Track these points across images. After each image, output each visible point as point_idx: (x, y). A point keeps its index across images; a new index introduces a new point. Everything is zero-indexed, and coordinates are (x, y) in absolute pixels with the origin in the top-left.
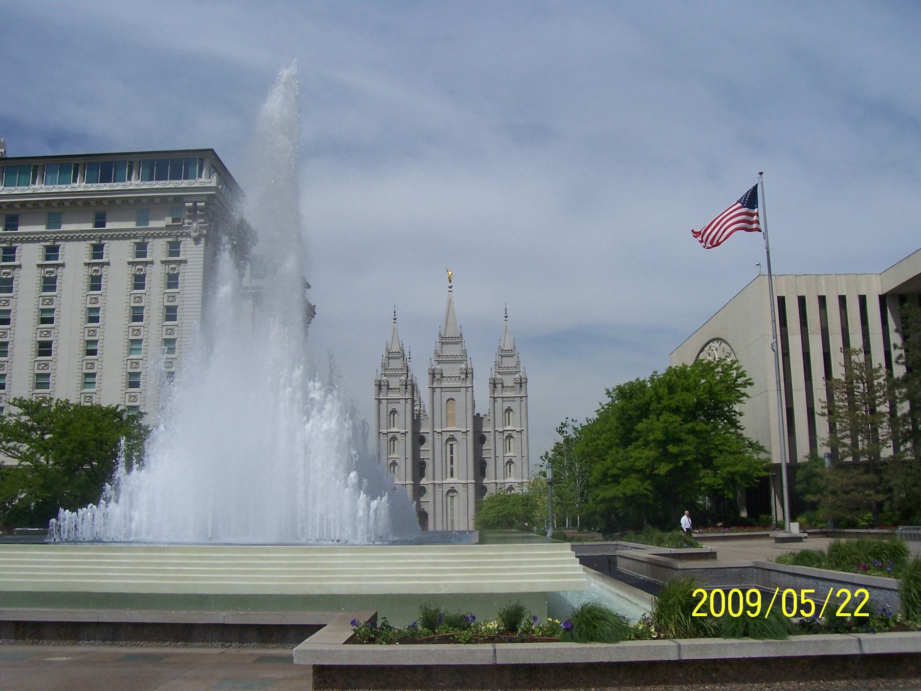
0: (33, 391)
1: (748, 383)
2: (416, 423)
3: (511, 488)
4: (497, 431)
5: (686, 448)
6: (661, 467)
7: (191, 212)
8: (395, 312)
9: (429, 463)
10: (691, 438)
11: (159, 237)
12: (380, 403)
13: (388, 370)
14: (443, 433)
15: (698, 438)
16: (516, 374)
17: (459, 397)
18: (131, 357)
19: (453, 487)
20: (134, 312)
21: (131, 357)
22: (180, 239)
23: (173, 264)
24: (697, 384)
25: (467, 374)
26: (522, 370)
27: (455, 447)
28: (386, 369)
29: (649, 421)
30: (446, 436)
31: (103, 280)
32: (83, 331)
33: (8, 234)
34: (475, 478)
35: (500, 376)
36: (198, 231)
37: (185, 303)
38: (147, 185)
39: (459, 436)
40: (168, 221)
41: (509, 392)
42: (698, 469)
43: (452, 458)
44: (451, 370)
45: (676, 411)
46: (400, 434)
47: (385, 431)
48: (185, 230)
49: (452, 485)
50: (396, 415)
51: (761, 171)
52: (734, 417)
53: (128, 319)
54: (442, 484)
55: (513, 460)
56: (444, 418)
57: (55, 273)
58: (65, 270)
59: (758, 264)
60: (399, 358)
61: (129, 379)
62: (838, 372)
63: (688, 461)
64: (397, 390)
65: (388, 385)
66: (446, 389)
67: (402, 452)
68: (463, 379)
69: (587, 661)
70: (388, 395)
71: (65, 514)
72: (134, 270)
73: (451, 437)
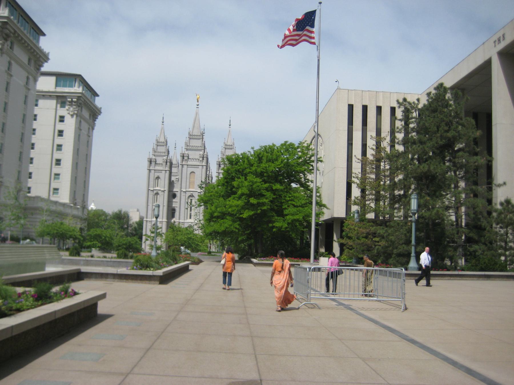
1: (319, 160)
2: (171, 184)
4: (182, 191)
5: (265, 200)
6: (245, 213)
9: (177, 210)
10: (268, 194)
14: (187, 192)
15: (274, 194)
16: (165, 156)
24: (278, 157)
25: (203, 158)
29: (239, 180)
30: (188, 194)
34: (168, 219)
42: (273, 216)
44: (193, 154)
45: (261, 175)
47: (152, 189)
51: (320, 1)
52: (308, 184)
54: (184, 222)
56: (188, 183)
59: (336, 81)
60: (163, 146)
62: (370, 153)
63: (264, 210)
65: (156, 162)
66: (190, 166)
68: (201, 161)
73: (191, 195)
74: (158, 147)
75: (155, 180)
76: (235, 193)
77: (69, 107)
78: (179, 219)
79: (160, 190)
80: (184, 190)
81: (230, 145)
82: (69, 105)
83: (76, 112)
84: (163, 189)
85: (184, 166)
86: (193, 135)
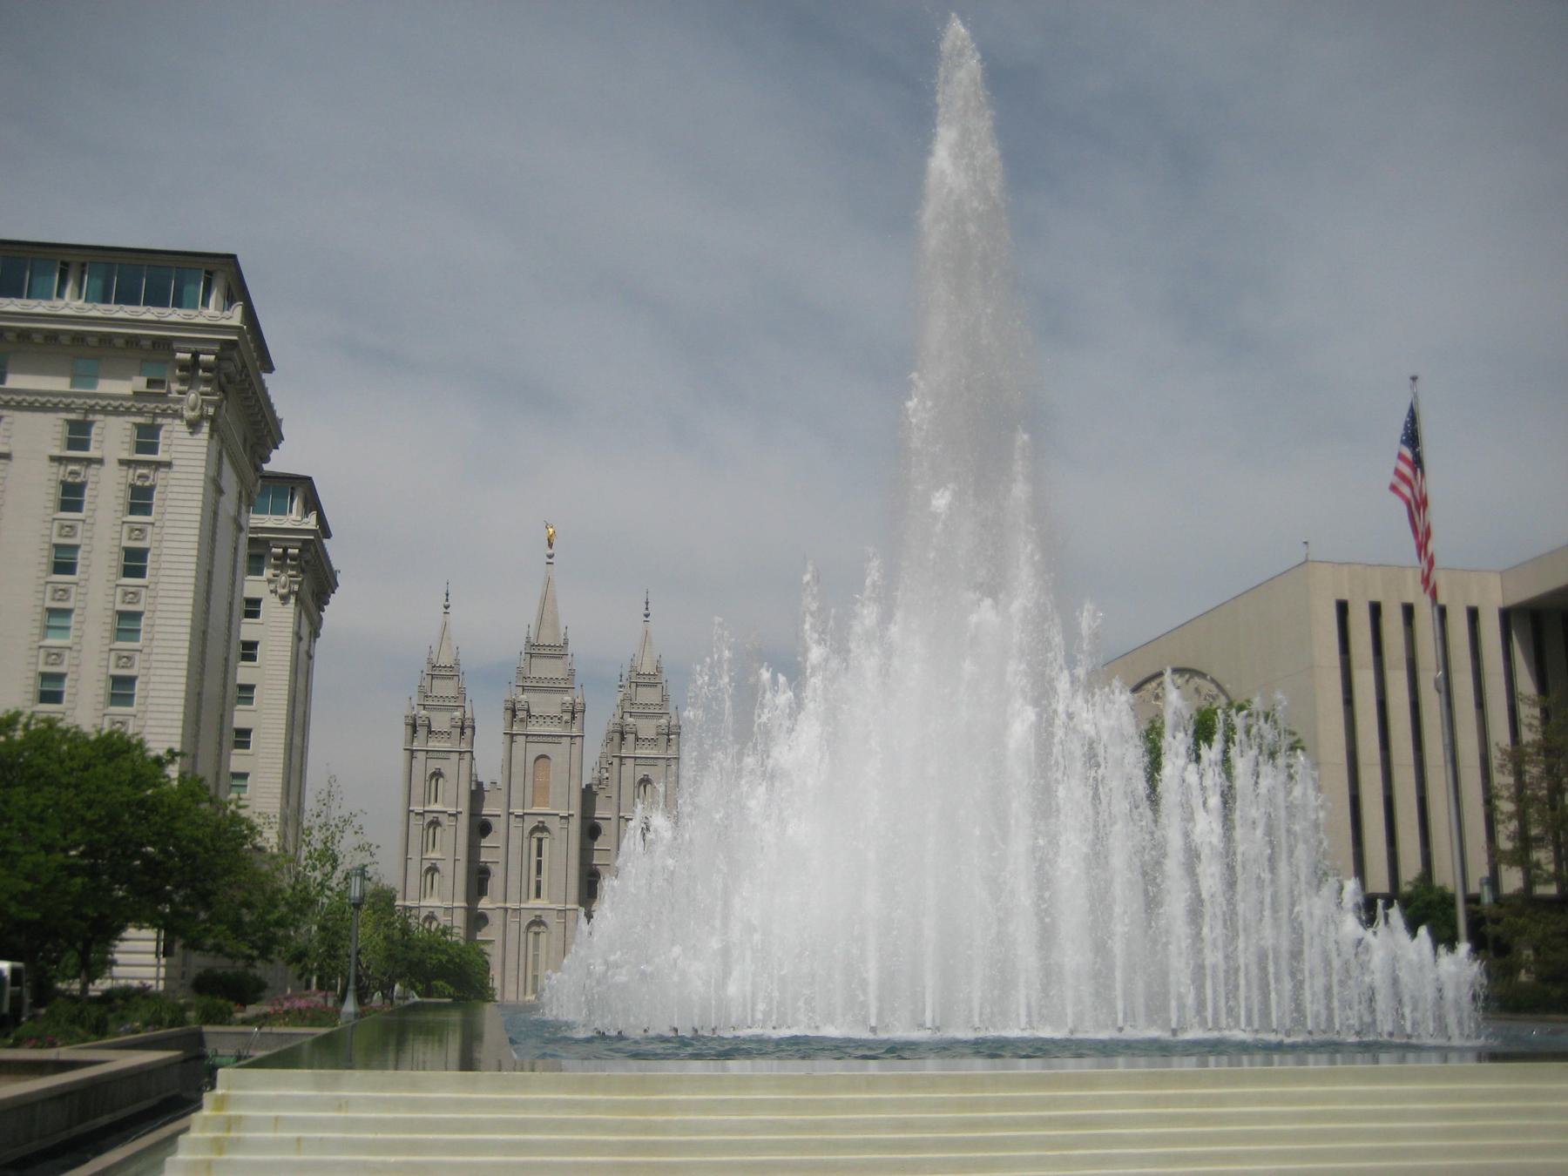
0: (104, 709)
3: (431, 918)
4: (413, 811)
7: (187, 371)
8: (447, 595)
11: (116, 412)
12: (412, 757)
13: (431, 699)
14: (426, 814)
16: (457, 710)
17: (558, 753)
18: (48, 642)
19: (540, 916)
20: (59, 555)
21: (48, 642)
22: (159, 421)
23: (144, 469)
25: (573, 713)
26: (672, 711)
27: (545, 844)
28: (427, 697)
30: (531, 823)
31: (87, 492)
32: (42, 589)
33: (78, 395)
34: (468, 900)
35: (632, 719)
36: (199, 407)
37: (165, 544)
38: (99, 310)
39: (554, 825)
40: (139, 383)
41: (646, 748)
43: (539, 864)
44: (541, 704)
46: (558, 818)
47: (419, 809)
48: (172, 405)
49: (538, 913)
50: (441, 781)
53: (114, 570)
55: (438, 866)
56: (529, 791)
57: (82, 476)
58: (172, 474)
61: (112, 689)
64: (446, 735)
65: (429, 726)
66: (535, 739)
67: (450, 847)
68: (566, 722)
70: (429, 744)
72: (62, 472)
73: (541, 825)
74: (435, 682)
75: (636, 790)
76: (137, 804)
77: (272, 571)
78: (505, 901)
79: (445, 812)
80: (519, 812)
81: (649, 674)
82: (276, 567)
83: (296, 588)
84: (452, 810)
85: (517, 738)
86: (539, 645)
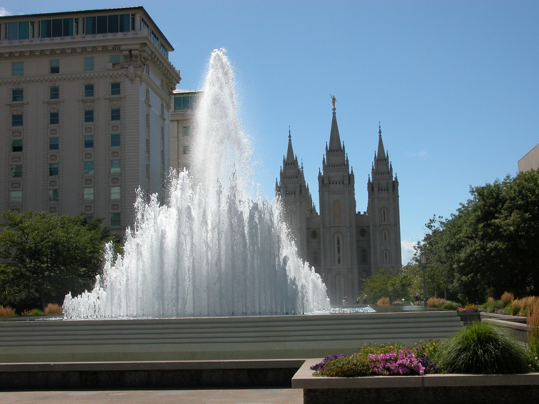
69: (485, 385)
71: (66, 295)
